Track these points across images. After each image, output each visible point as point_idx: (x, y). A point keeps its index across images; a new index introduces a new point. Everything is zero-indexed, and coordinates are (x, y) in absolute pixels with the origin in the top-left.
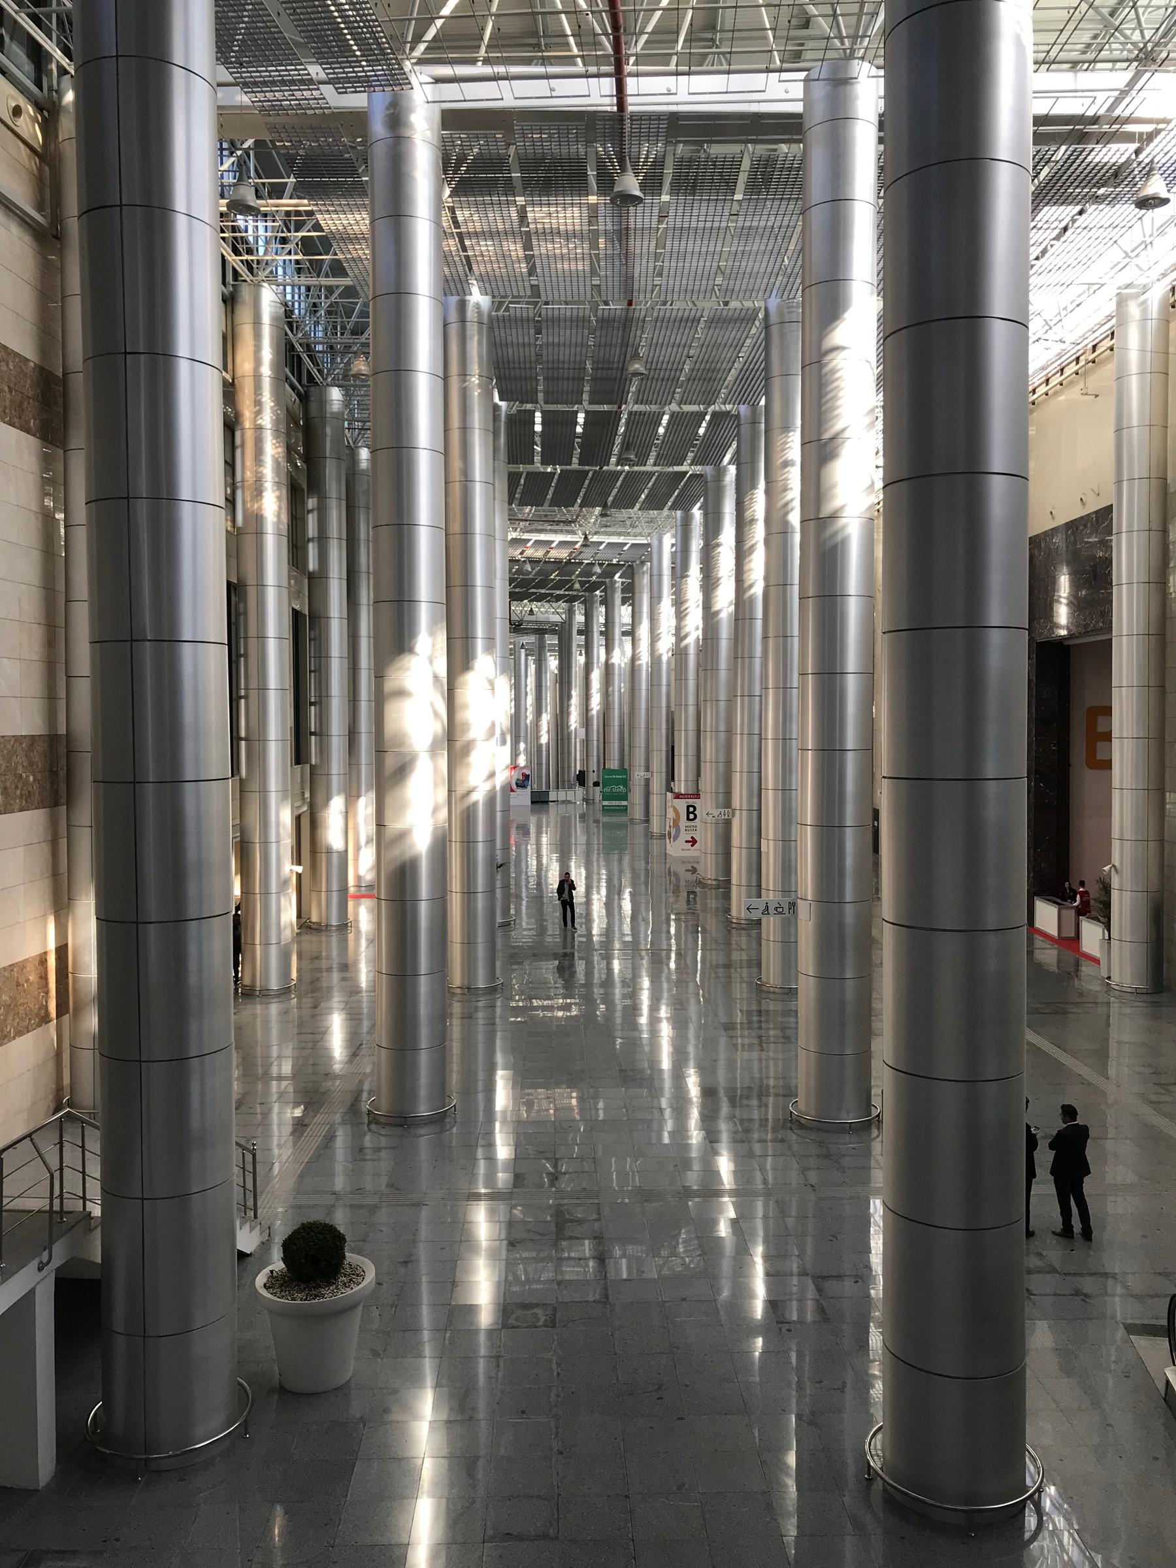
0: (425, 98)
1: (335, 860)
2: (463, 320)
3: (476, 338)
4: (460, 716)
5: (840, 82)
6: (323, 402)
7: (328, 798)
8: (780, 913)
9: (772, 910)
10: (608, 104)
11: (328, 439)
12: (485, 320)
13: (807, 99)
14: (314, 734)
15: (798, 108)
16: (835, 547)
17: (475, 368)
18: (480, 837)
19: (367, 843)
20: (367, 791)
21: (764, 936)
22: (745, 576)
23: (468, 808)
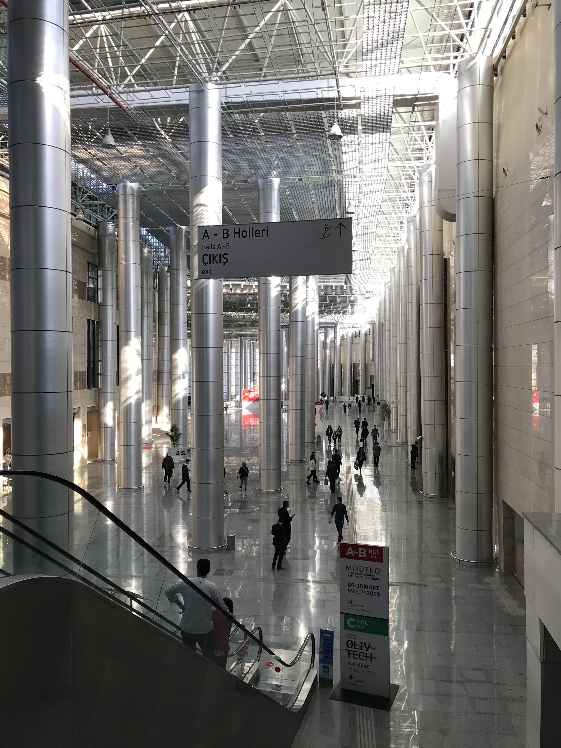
0: (214, 97)
1: (109, 430)
2: (125, 194)
3: (131, 200)
4: (123, 365)
5: (200, 92)
6: (105, 229)
7: (106, 402)
8: (184, 454)
9: (180, 453)
10: (337, 96)
11: (107, 245)
12: (135, 193)
13: (190, 100)
14: (100, 374)
15: (187, 102)
16: (202, 289)
17: (130, 215)
18: (133, 421)
19: (146, 423)
20: (146, 400)
21: (424, 470)
22: (292, 302)
23: (127, 406)
